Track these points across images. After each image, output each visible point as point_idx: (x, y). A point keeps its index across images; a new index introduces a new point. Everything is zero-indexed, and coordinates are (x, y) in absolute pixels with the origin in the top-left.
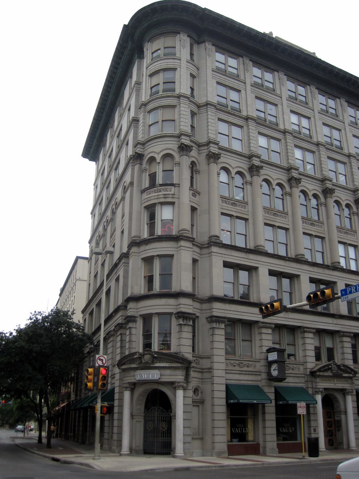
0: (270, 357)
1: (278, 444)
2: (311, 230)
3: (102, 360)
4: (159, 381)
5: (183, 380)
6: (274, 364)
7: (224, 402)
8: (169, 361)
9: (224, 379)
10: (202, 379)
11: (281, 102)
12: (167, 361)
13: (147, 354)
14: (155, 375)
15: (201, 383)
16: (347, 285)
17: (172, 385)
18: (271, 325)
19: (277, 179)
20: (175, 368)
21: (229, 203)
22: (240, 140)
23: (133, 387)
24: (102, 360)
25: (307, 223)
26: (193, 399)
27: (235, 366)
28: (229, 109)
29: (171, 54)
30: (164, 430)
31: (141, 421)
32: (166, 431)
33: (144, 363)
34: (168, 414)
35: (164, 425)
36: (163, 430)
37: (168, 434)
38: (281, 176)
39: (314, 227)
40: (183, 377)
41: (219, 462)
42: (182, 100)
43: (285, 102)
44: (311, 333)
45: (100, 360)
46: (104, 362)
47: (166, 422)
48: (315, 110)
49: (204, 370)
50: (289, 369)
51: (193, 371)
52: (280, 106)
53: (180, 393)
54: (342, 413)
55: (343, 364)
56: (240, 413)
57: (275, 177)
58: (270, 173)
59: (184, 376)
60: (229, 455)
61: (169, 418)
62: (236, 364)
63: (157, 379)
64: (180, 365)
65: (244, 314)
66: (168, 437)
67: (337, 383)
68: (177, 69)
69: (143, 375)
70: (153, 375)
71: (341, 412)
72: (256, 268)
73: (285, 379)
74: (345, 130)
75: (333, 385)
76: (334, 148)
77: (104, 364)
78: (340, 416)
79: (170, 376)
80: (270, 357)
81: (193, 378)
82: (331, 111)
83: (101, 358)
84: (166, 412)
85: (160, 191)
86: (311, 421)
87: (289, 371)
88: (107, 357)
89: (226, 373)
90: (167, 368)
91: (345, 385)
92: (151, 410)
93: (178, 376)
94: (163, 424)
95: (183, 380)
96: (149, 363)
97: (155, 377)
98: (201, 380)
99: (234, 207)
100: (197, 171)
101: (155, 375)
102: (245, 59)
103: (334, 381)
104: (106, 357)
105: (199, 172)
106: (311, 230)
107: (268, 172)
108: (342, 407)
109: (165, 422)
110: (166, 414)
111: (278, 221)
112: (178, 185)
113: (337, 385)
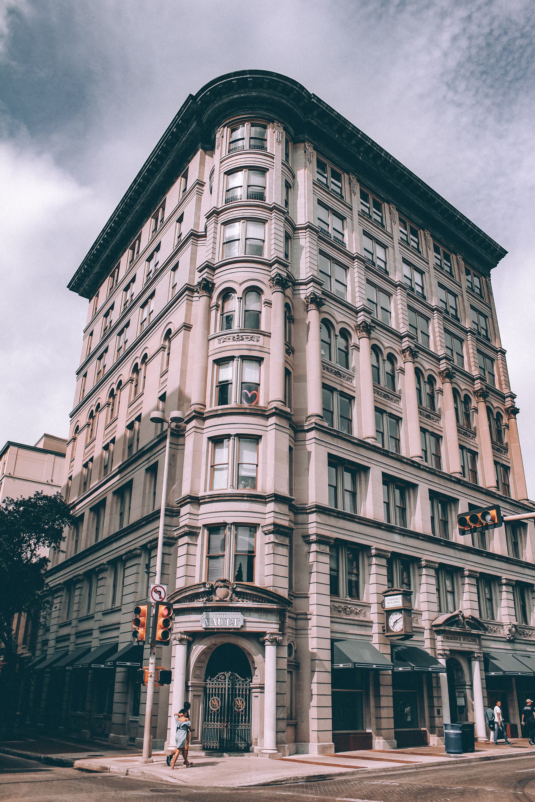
0: (388, 603)
1: (334, 735)
2: (428, 425)
3: (159, 593)
4: (244, 630)
5: (276, 631)
6: (394, 614)
7: (328, 666)
8: (258, 599)
9: (329, 631)
10: (296, 630)
11: (392, 244)
12: (255, 599)
13: (221, 587)
14: (235, 620)
15: (294, 636)
16: (471, 507)
17: (258, 638)
18: (387, 554)
19: (388, 347)
20: (272, 611)
21: (331, 371)
22: (328, 276)
23: (191, 639)
24: (159, 593)
25: (330, 370)
26: (288, 661)
27: (340, 611)
28: (332, 239)
29: (259, 143)
30: (215, 709)
31: (200, 696)
32: (218, 711)
33: (217, 601)
34: (246, 685)
35: (240, 703)
36: (214, 709)
37: (245, 717)
38: (433, 366)
39: (430, 421)
40: (277, 626)
41: (418, 761)
42: (356, 263)
43: (397, 245)
44: (432, 568)
45: (156, 592)
46: (163, 595)
47: (218, 697)
48: (394, 237)
49: (299, 617)
50: (351, 613)
51: (289, 617)
52: (390, 249)
53: (270, 650)
54: (467, 687)
55: (472, 617)
56: (352, 687)
57: (386, 345)
58: (383, 339)
59: (278, 623)
60: (336, 751)
61: (248, 691)
62: (340, 609)
63: (239, 627)
64: (275, 607)
65: (354, 534)
66: (245, 722)
67: (463, 643)
68: (268, 169)
69: (214, 620)
70: (219, 620)
71: (466, 685)
72: (366, 469)
73: (411, 636)
74: (462, 296)
75: (459, 645)
76: (415, 295)
77: (163, 599)
78: (463, 692)
79: (256, 624)
80: (388, 603)
81: (288, 627)
82: (412, 243)
83: (159, 589)
84: (243, 682)
85: (243, 340)
86: (381, 697)
87: (351, 615)
88: (168, 588)
89: (331, 622)
90: (254, 611)
91: (473, 647)
92: (218, 678)
93: (269, 626)
94: (213, 700)
95: (276, 631)
96: (226, 601)
97: (235, 625)
98: (294, 632)
99: (337, 378)
100: (291, 319)
101: (235, 620)
102: (307, 144)
103: (460, 640)
104: (165, 587)
105: (293, 321)
106: (428, 425)
107: (378, 336)
108: (467, 679)
109: (241, 698)
110: (243, 685)
111: (392, 407)
112: (268, 335)
113: (463, 645)
